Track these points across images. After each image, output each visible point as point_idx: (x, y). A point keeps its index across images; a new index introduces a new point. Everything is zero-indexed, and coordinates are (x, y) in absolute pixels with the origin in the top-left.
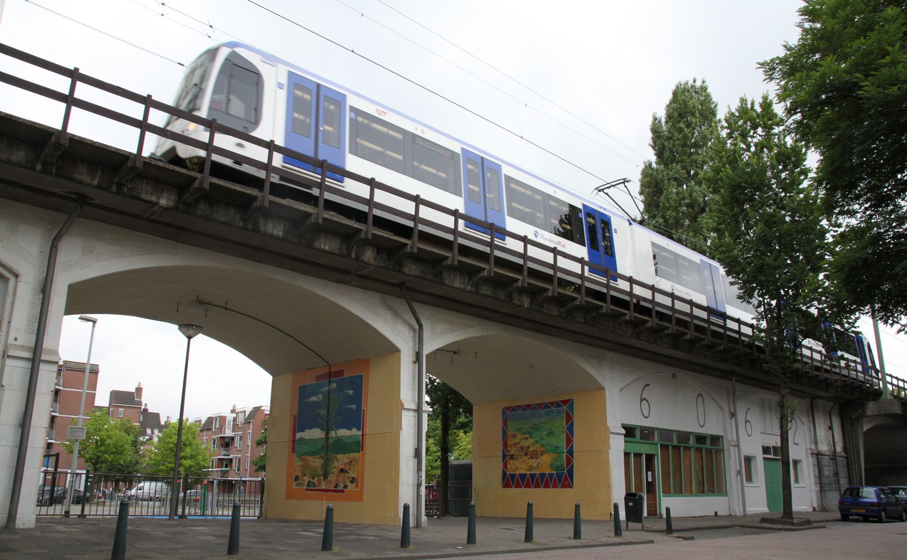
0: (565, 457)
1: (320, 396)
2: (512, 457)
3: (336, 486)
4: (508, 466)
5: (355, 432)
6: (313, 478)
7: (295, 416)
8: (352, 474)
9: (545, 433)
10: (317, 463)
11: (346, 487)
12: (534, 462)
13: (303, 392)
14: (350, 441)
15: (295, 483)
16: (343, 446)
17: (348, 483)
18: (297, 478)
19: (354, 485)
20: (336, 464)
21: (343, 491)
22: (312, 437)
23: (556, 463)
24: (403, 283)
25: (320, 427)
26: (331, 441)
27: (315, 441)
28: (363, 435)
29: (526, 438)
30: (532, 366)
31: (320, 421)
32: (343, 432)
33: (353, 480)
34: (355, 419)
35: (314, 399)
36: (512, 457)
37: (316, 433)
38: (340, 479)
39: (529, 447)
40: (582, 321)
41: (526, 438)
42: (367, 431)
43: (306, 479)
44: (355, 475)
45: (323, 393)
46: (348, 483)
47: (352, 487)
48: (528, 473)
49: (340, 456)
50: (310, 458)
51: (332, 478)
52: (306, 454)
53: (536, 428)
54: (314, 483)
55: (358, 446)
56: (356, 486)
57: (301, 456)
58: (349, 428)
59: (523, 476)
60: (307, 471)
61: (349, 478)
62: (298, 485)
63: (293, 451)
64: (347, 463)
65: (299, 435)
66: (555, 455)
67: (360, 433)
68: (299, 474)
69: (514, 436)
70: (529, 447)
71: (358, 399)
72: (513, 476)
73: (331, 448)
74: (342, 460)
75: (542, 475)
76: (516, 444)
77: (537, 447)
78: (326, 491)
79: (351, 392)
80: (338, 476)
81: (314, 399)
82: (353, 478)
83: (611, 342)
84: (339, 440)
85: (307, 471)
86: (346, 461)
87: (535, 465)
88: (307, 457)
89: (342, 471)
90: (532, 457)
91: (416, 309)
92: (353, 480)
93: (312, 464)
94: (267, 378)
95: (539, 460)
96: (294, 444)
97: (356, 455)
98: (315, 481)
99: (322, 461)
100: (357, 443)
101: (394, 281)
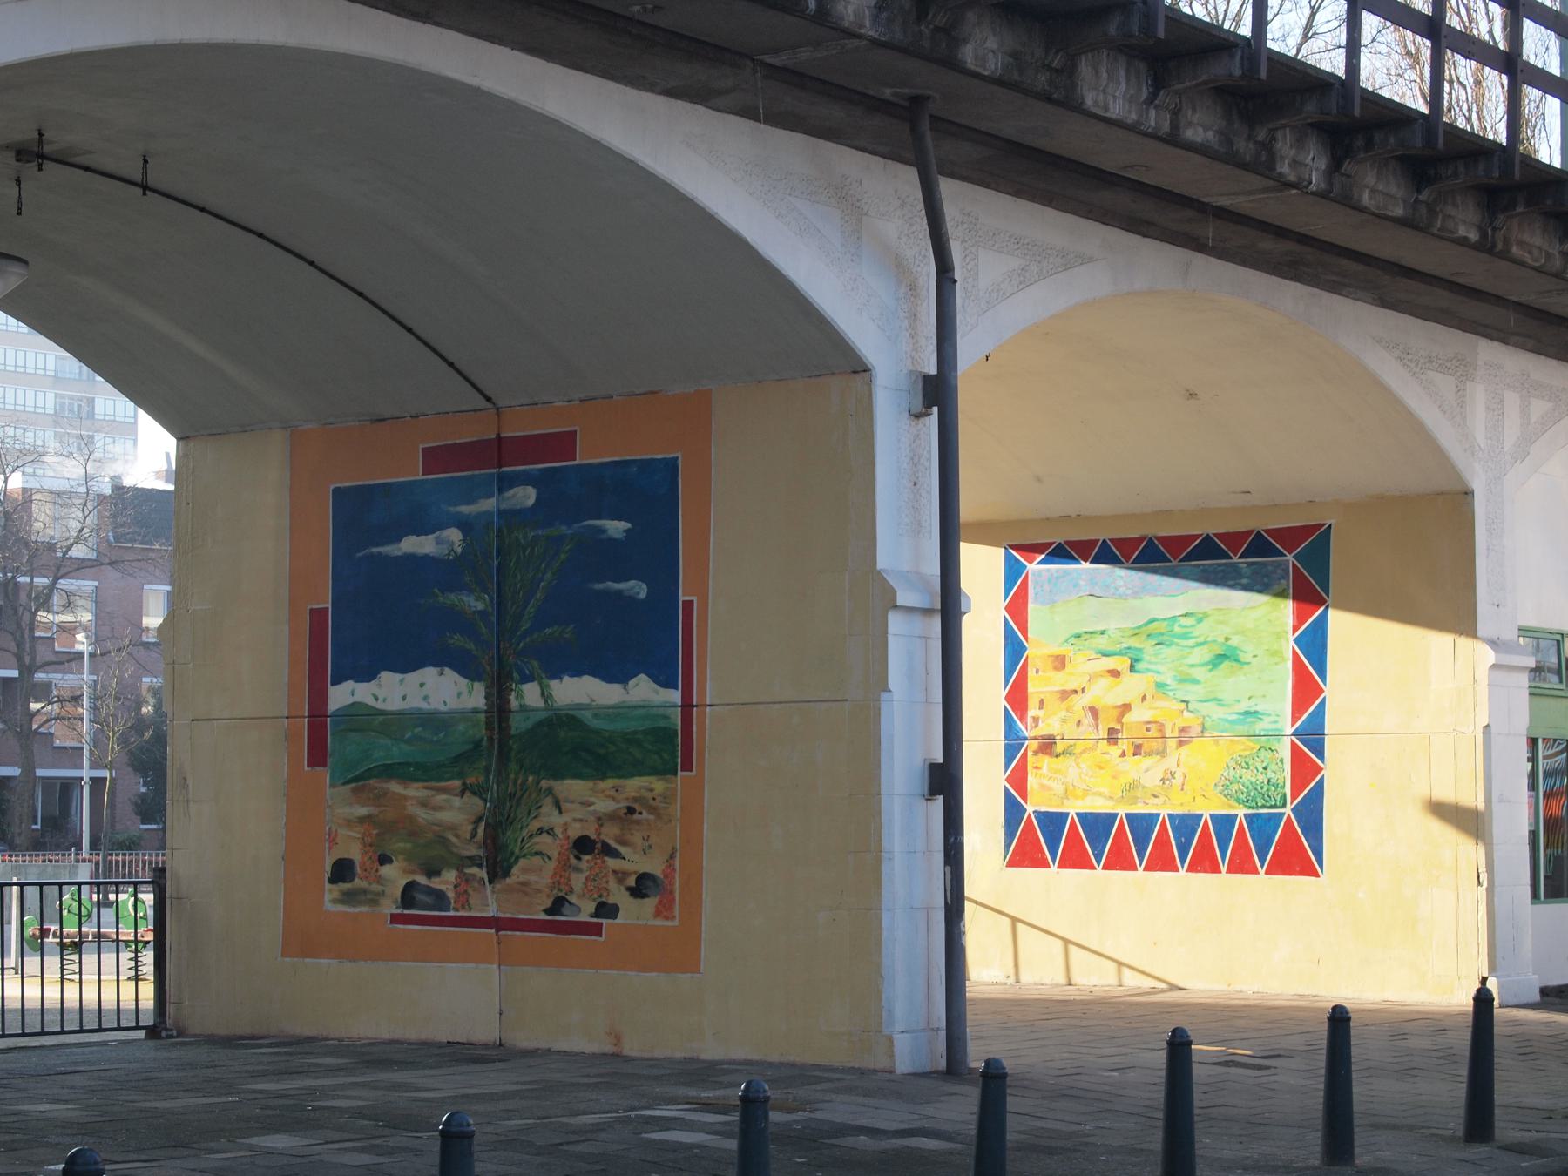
0: (1286, 754)
1: (454, 535)
2: (1047, 745)
3: (558, 905)
4: (1032, 782)
5: (643, 689)
6: (432, 872)
7: (317, 616)
8: (636, 862)
9: (1203, 654)
10: (453, 812)
11: (606, 910)
12: (1147, 770)
13: (361, 517)
14: (619, 726)
15: (331, 892)
16: (578, 748)
17: (618, 896)
18: (342, 870)
19: (650, 903)
20: (549, 816)
21: (596, 930)
22: (415, 703)
23: (1248, 776)
24: (917, 101)
25: (466, 667)
26: (518, 724)
27: (432, 721)
28: (687, 706)
29: (1115, 673)
30: (1192, 395)
31: (457, 640)
32: (579, 691)
33: (642, 887)
34: (652, 637)
35: (413, 545)
36: (1047, 745)
37: (441, 691)
38: (578, 881)
39: (1126, 708)
40: (1474, 236)
41: (1115, 673)
42: (712, 687)
43: (395, 876)
44: (655, 867)
45: (465, 525)
46: (618, 896)
47: (634, 913)
48: (1121, 811)
49: (572, 788)
50: (415, 791)
51: (535, 875)
52: (389, 771)
53: (1159, 634)
54: (439, 898)
55: (666, 748)
56: (663, 911)
57: (360, 778)
58: (619, 675)
59: (1097, 824)
60: (398, 845)
61: (621, 876)
62: (349, 898)
63: (317, 755)
64: (612, 817)
65: (341, 695)
66: (1244, 747)
67: (676, 696)
68: (355, 853)
69: (1060, 662)
70: (1126, 708)
71: (657, 550)
72: (1053, 822)
73: (515, 758)
74: (582, 802)
75: (1186, 824)
76: (1065, 695)
77: (1166, 711)
78: (496, 923)
79: (616, 528)
80: (565, 866)
81: (413, 545)
82: (643, 878)
83: (1518, 306)
84: (562, 722)
85: (398, 845)
86: (603, 806)
87: (1152, 780)
88: (395, 787)
89: (583, 845)
90: (1137, 750)
91: (951, 213)
92: (642, 887)
93: (423, 815)
94: (173, 441)
95: (1170, 762)
96: (319, 736)
97: (658, 785)
98: (446, 881)
99: (476, 804)
100: (663, 736)
101: (887, 93)
